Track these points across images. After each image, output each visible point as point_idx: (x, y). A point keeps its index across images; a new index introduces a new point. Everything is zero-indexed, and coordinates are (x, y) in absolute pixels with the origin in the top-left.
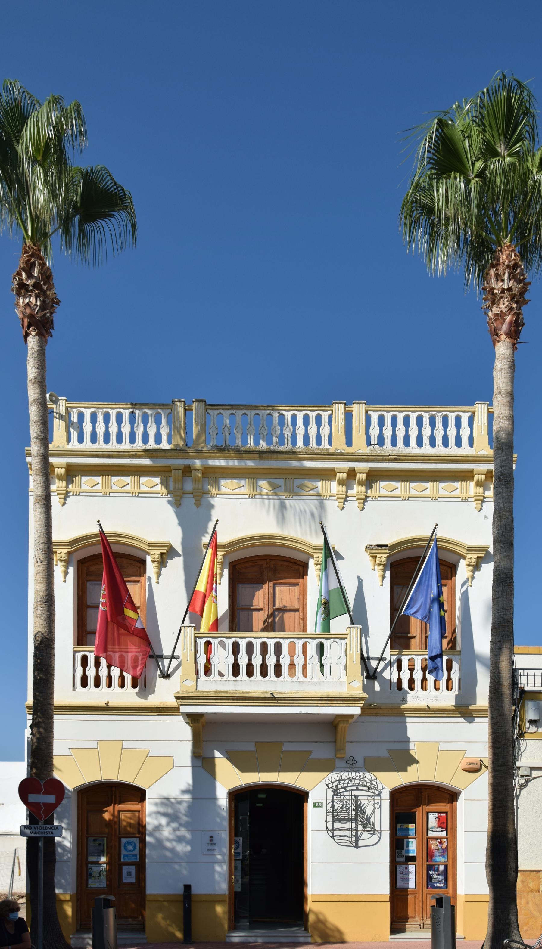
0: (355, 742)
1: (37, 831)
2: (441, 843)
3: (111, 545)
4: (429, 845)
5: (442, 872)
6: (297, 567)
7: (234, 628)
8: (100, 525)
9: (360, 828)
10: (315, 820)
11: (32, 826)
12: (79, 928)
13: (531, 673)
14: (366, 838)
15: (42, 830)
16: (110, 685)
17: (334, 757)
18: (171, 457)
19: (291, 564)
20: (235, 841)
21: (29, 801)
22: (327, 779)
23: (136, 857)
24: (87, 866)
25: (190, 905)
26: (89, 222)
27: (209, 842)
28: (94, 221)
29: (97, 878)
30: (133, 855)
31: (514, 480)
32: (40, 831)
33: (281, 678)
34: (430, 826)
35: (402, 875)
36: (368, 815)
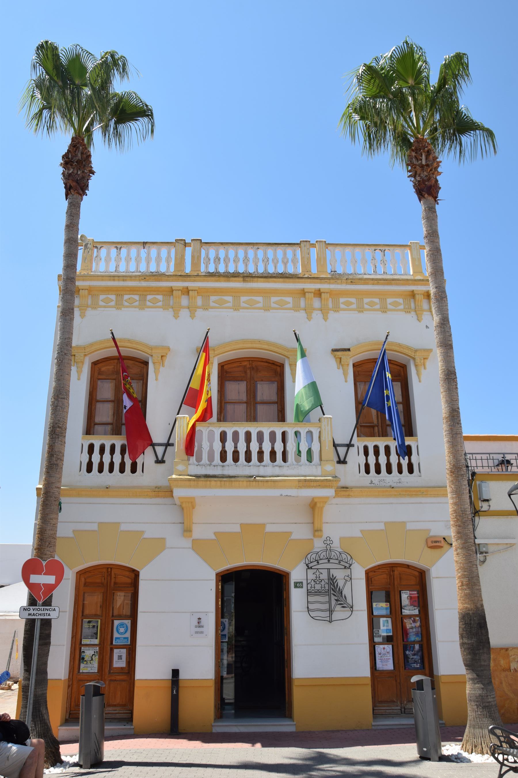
0: (330, 523)
1: (35, 612)
2: (414, 621)
3: (120, 348)
4: (404, 624)
5: (418, 652)
6: (275, 367)
7: (222, 419)
8: (112, 333)
9: (333, 602)
10: (297, 598)
11: (31, 608)
12: (67, 718)
13: (478, 457)
14: (339, 613)
15: (40, 612)
16: (400, 471)
17: (312, 537)
18: (172, 281)
19: (270, 365)
20: (222, 622)
21: (30, 582)
22: (307, 559)
23: (128, 640)
24: (80, 649)
25: (177, 691)
26: (121, 124)
27: (197, 624)
28: (124, 123)
29: (89, 662)
30: (125, 638)
31: (448, 297)
32: (38, 612)
33: (263, 464)
34: (403, 604)
35: (380, 656)
36: (339, 588)
